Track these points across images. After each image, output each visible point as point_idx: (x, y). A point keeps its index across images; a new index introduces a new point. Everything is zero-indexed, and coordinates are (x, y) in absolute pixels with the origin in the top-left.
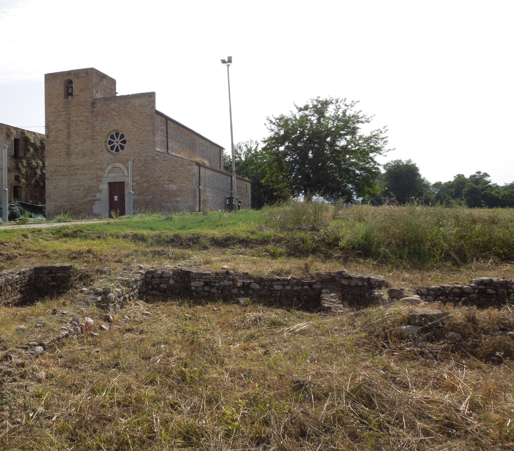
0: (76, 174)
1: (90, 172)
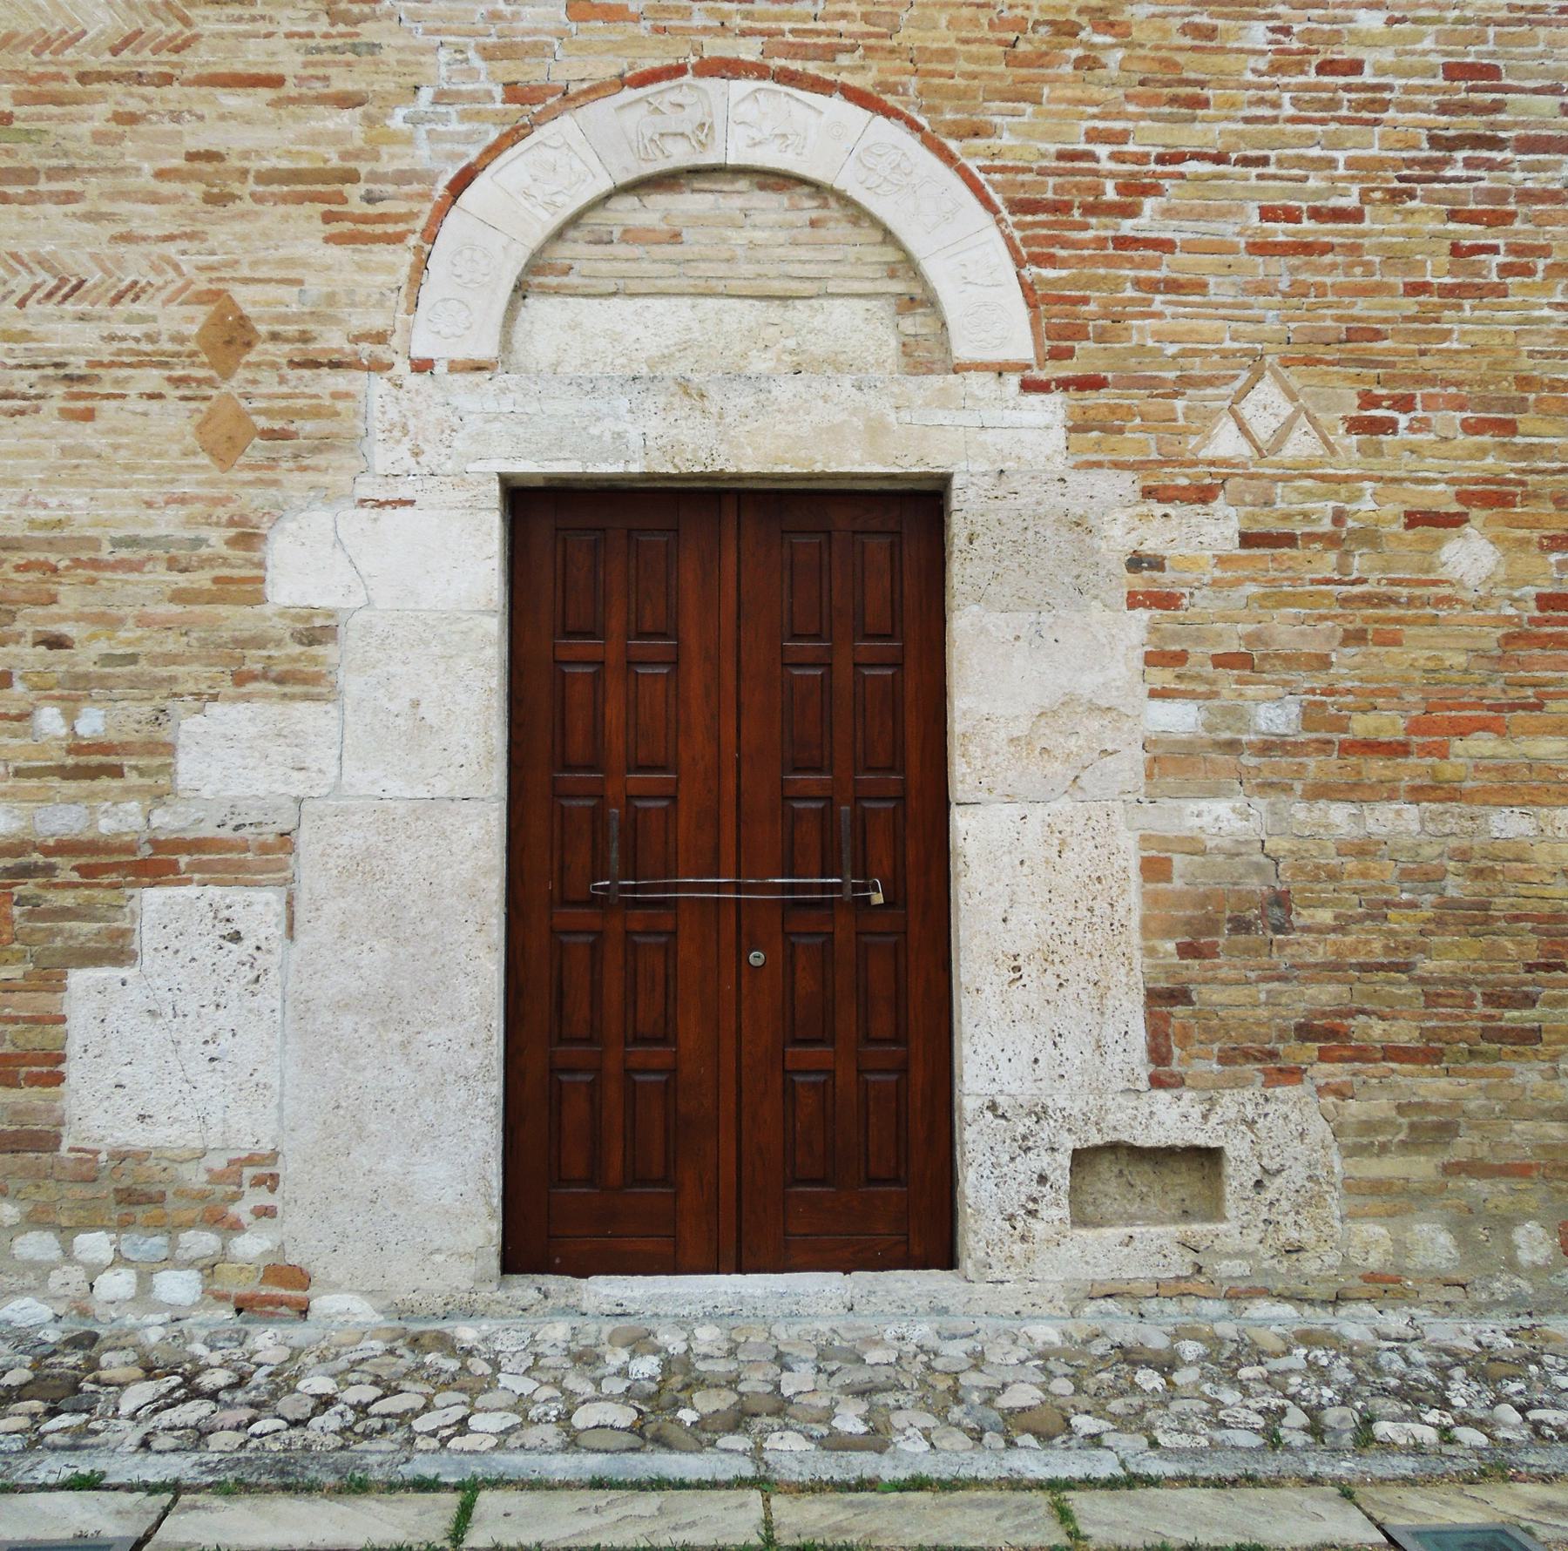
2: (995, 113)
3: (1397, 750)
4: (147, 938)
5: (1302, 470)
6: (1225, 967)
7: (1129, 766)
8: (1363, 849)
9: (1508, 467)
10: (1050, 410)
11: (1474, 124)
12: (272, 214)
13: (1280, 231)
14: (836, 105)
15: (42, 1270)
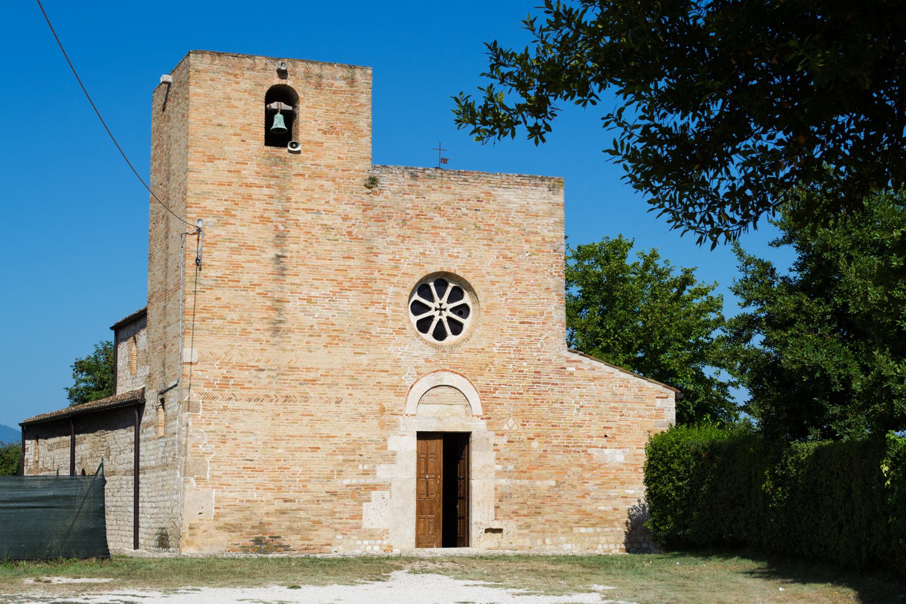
0: (306, 399)
1: (358, 394)
2: (478, 378)
3: (525, 472)
4: (373, 499)
5: (515, 431)
6: (504, 503)
7: (493, 474)
8: (521, 486)
9: (540, 431)
10: (484, 422)
11: (538, 380)
12: (388, 391)
13: (513, 396)
14: (458, 376)
15: (359, 545)
